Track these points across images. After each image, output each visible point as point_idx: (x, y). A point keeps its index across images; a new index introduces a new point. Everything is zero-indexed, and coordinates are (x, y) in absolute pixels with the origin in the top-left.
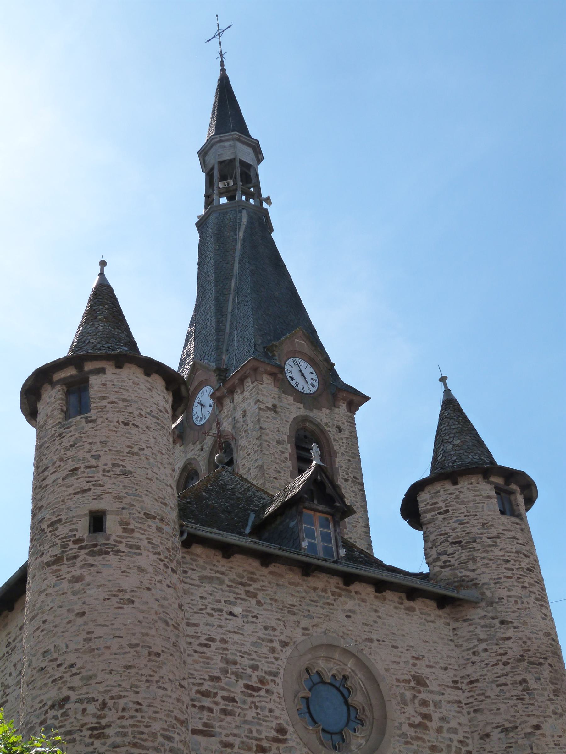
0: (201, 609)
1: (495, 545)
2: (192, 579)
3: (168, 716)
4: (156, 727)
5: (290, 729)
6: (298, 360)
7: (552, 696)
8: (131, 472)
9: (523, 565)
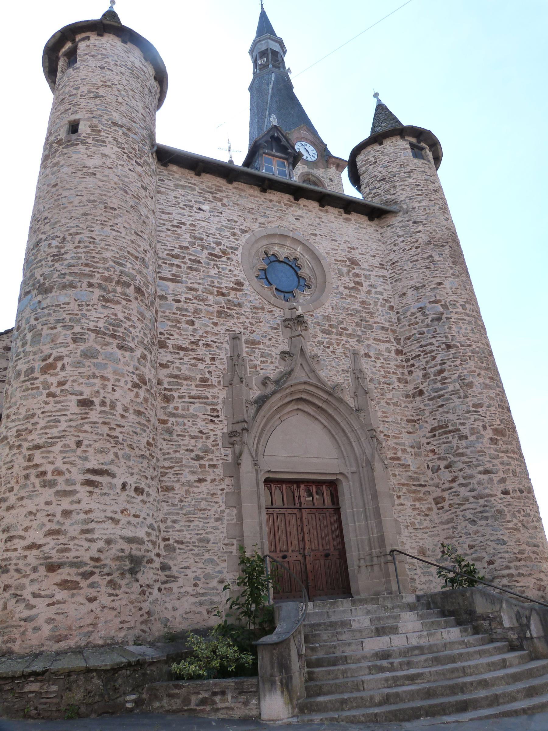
1: (410, 176)
4: (108, 254)
5: (246, 283)
6: (303, 143)
8: (103, 97)
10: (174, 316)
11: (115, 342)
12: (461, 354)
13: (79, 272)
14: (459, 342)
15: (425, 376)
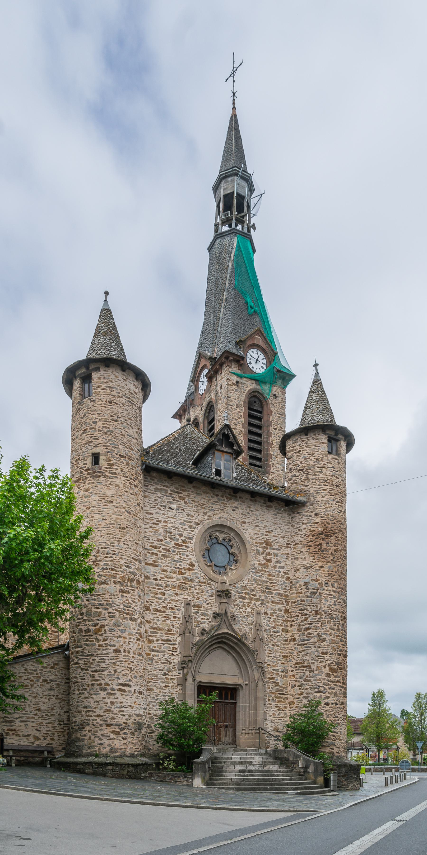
0: (154, 506)
2: (150, 490)
3: (129, 557)
5: (197, 564)
7: (333, 553)
8: (112, 431)
9: (334, 483)
11: (128, 617)
12: (323, 619)
13: (109, 574)
14: (323, 611)
15: (299, 630)
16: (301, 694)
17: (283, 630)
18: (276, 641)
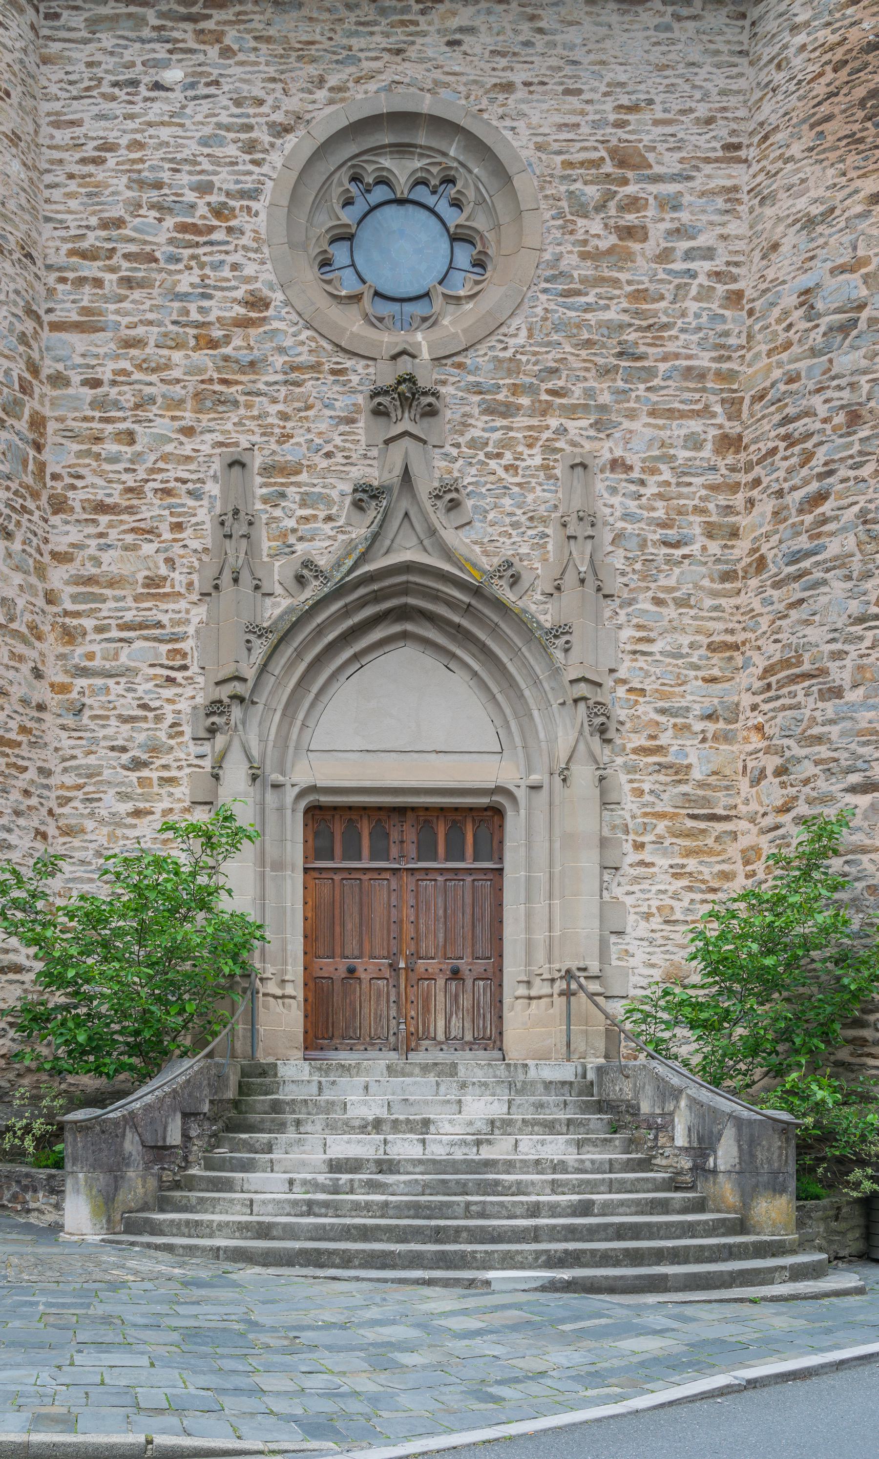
0: (88, 89)
2: (70, 29)
10: (85, 425)
16: (785, 809)
17: (710, 532)
18: (672, 582)
